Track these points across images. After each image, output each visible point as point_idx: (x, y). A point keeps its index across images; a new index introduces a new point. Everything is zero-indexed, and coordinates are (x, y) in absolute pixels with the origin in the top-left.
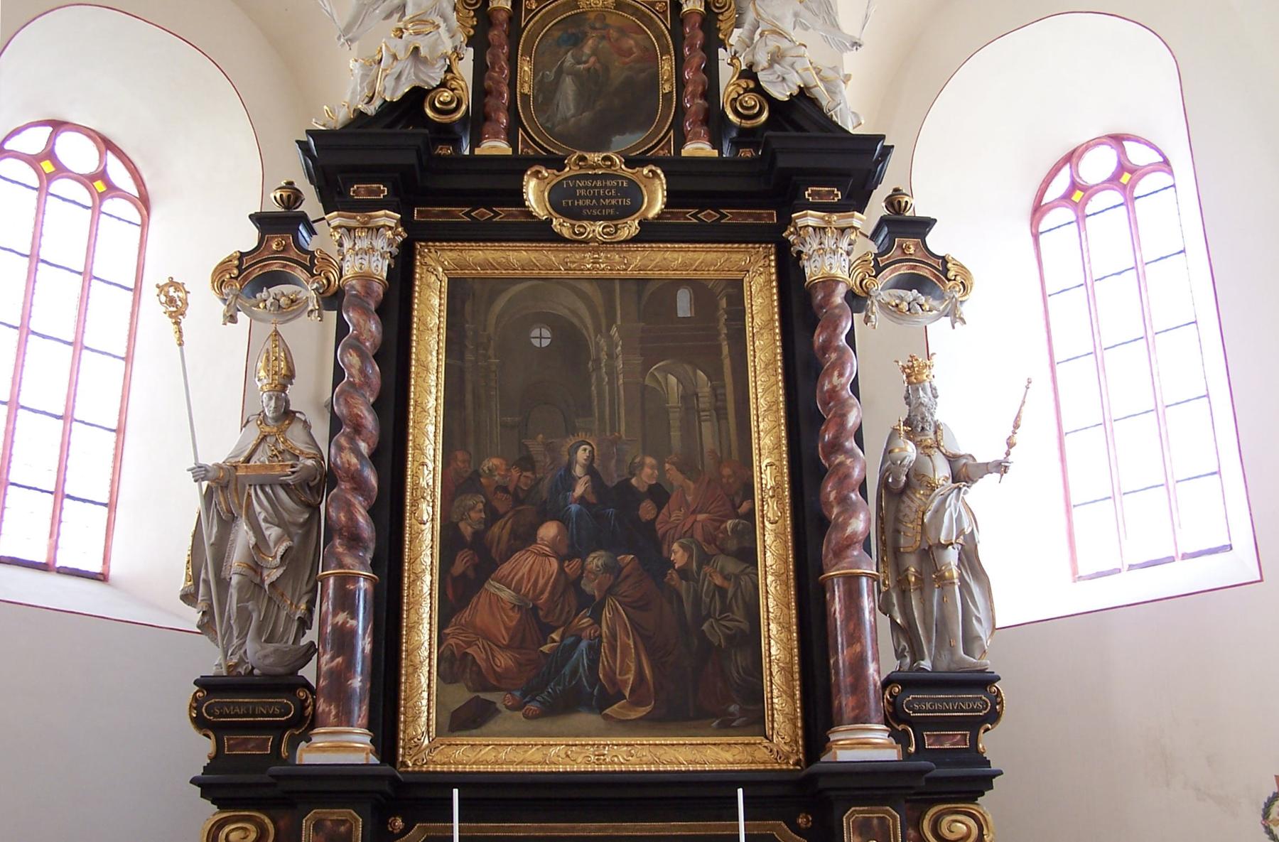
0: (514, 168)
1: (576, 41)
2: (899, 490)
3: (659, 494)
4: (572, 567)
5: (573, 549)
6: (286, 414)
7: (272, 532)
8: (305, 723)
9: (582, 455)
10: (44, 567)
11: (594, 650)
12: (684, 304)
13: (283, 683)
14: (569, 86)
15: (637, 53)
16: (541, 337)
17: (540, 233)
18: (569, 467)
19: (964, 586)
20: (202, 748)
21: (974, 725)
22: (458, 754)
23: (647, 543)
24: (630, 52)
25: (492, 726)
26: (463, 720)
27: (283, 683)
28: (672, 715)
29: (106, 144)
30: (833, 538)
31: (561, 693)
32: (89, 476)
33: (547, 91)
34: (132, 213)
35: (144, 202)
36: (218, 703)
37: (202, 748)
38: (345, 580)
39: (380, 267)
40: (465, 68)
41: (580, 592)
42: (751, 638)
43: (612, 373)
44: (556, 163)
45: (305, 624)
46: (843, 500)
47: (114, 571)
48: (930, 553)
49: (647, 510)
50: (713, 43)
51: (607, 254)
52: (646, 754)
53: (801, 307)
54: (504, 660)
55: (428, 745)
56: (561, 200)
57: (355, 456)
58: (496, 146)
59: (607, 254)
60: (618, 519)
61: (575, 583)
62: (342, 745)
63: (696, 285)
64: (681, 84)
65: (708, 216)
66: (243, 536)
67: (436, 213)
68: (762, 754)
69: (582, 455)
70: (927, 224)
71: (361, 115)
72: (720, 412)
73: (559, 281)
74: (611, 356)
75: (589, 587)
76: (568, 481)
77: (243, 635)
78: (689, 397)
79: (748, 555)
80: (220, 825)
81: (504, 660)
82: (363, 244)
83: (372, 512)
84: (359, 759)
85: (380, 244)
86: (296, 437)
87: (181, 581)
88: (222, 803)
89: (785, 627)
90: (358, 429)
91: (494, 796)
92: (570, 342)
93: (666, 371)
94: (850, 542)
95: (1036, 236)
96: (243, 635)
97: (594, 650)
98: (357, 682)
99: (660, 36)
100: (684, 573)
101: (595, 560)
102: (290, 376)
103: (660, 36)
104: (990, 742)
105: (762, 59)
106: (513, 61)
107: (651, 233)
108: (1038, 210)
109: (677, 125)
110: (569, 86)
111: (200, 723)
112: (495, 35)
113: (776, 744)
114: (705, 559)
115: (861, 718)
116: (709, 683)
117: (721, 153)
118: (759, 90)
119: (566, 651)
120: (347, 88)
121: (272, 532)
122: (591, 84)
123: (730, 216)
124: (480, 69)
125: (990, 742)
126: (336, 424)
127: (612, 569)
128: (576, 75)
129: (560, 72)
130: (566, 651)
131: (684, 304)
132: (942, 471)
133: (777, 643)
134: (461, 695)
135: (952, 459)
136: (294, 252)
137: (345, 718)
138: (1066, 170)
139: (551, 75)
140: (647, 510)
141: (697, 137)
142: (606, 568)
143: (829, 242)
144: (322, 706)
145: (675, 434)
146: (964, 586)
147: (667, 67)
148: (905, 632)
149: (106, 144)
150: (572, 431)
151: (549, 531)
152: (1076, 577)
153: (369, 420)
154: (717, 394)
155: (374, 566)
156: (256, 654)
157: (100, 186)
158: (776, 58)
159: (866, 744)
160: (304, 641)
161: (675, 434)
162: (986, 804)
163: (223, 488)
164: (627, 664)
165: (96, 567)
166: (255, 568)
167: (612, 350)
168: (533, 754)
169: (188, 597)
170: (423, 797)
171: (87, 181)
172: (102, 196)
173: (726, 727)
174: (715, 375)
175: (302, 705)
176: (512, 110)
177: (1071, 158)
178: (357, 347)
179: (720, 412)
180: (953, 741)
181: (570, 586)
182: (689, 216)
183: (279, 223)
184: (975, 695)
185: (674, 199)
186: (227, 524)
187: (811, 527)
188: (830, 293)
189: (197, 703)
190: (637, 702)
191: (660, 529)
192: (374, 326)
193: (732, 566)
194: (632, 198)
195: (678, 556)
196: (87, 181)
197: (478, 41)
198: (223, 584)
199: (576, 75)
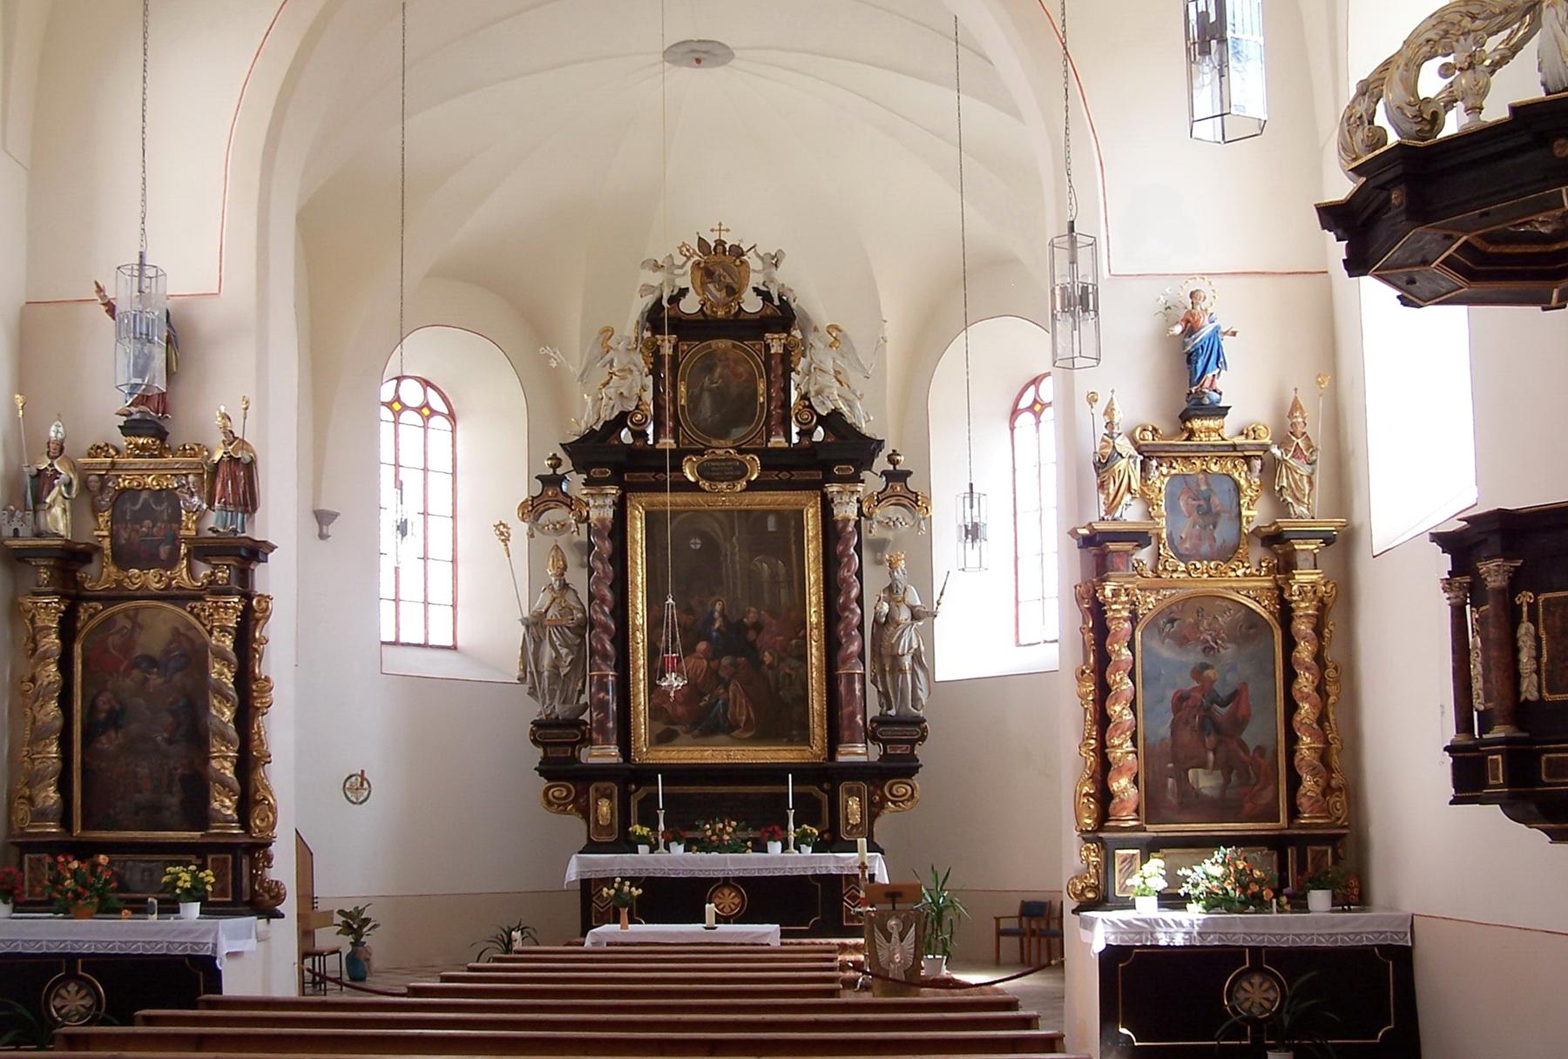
0: (678, 455)
1: (710, 369)
2: (884, 625)
3: (758, 626)
4: (714, 664)
5: (714, 655)
6: (565, 586)
7: (564, 651)
8: (587, 741)
9: (718, 607)
10: (425, 646)
11: (726, 704)
12: (771, 524)
13: (574, 723)
14: (706, 397)
15: (745, 376)
16: (696, 544)
17: (694, 487)
18: (712, 613)
19: (914, 674)
20: (539, 752)
21: (913, 743)
22: (661, 754)
23: (752, 651)
24: (741, 375)
25: (677, 741)
26: (662, 738)
27: (574, 723)
28: (765, 735)
29: (426, 383)
30: (842, 654)
31: (709, 725)
32: (441, 591)
33: (694, 400)
34: (446, 424)
35: (452, 416)
36: (543, 731)
37: (539, 752)
38: (602, 677)
39: (609, 513)
40: (648, 396)
41: (649, 843)
42: (804, 699)
43: (733, 561)
44: (700, 453)
45: (582, 692)
46: (848, 635)
47: (459, 644)
48: (896, 658)
49: (752, 635)
50: (788, 369)
51: (729, 496)
52: (751, 755)
53: (831, 530)
54: (680, 710)
55: (646, 752)
56: (703, 472)
57: (603, 615)
58: (668, 443)
59: (729, 496)
60: (737, 640)
61: (716, 672)
62: (605, 754)
63: (776, 512)
64: (769, 398)
65: (784, 475)
66: (548, 653)
67: (637, 476)
68: (808, 754)
69: (718, 607)
70: (909, 473)
71: (592, 431)
72: (790, 583)
73: (705, 512)
74: (733, 554)
75: (722, 673)
76: (712, 620)
77: (552, 698)
78: (774, 576)
79: (803, 657)
80: (548, 789)
81: (680, 710)
82: (600, 502)
83: (612, 641)
84: (614, 760)
85: (609, 501)
86: (570, 596)
87: (516, 672)
88: (549, 780)
89: (820, 695)
90: (603, 601)
91: (675, 774)
92: (711, 547)
93: (761, 561)
94: (850, 656)
95: (1012, 430)
96: (552, 698)
97: (726, 704)
98: (611, 725)
99: (758, 366)
100: (770, 666)
101: (726, 661)
102: (565, 568)
103: (758, 366)
104: (919, 750)
105: (812, 390)
106: (674, 386)
107: (752, 487)
108: (1015, 412)
109: (767, 423)
110: (706, 397)
111: (535, 742)
112: (666, 373)
113: (814, 751)
114: (781, 660)
115: (853, 741)
116: (783, 721)
117: (789, 439)
118: (811, 406)
119: (712, 705)
120: (585, 415)
121: (564, 651)
122: (719, 396)
123: (797, 476)
124: (657, 395)
125: (919, 750)
126: (591, 597)
127: (734, 665)
128: (709, 390)
129: (702, 390)
130: (712, 705)
131: (771, 524)
132: (904, 615)
133: (817, 702)
134: (660, 727)
135: (912, 608)
136: (561, 497)
137: (607, 742)
138: (1032, 388)
139: (696, 391)
140: (752, 635)
141: (777, 434)
142: (732, 664)
143: (846, 498)
144: (595, 735)
145: (766, 596)
146: (914, 674)
147: (762, 387)
148: (884, 695)
149: (426, 383)
150: (713, 594)
151: (702, 646)
152: (1018, 644)
153: (609, 595)
154: (789, 573)
155: (616, 668)
156: (560, 710)
157: (426, 411)
158: (818, 393)
159: (858, 752)
160: (582, 702)
161: (766, 596)
162: (916, 780)
163: (535, 625)
164: (742, 712)
165: (450, 644)
166: (555, 666)
167: (734, 551)
168: (697, 755)
169: (522, 680)
170: (645, 775)
171: (418, 410)
172: (428, 418)
173: (791, 742)
174: (787, 563)
175: (584, 733)
176: (675, 417)
177: (1036, 381)
178: (599, 556)
179: (790, 583)
180: (901, 749)
181: (713, 673)
182: (774, 476)
183: (551, 481)
184: (911, 729)
185: (764, 467)
186: (538, 643)
187: (832, 646)
188: (845, 526)
189: (533, 733)
190: (746, 730)
191: (759, 645)
192: (607, 545)
193: (794, 663)
194: (742, 471)
195: (767, 658)
196: (418, 410)
197: (655, 372)
198: (540, 674)
199: (709, 390)
